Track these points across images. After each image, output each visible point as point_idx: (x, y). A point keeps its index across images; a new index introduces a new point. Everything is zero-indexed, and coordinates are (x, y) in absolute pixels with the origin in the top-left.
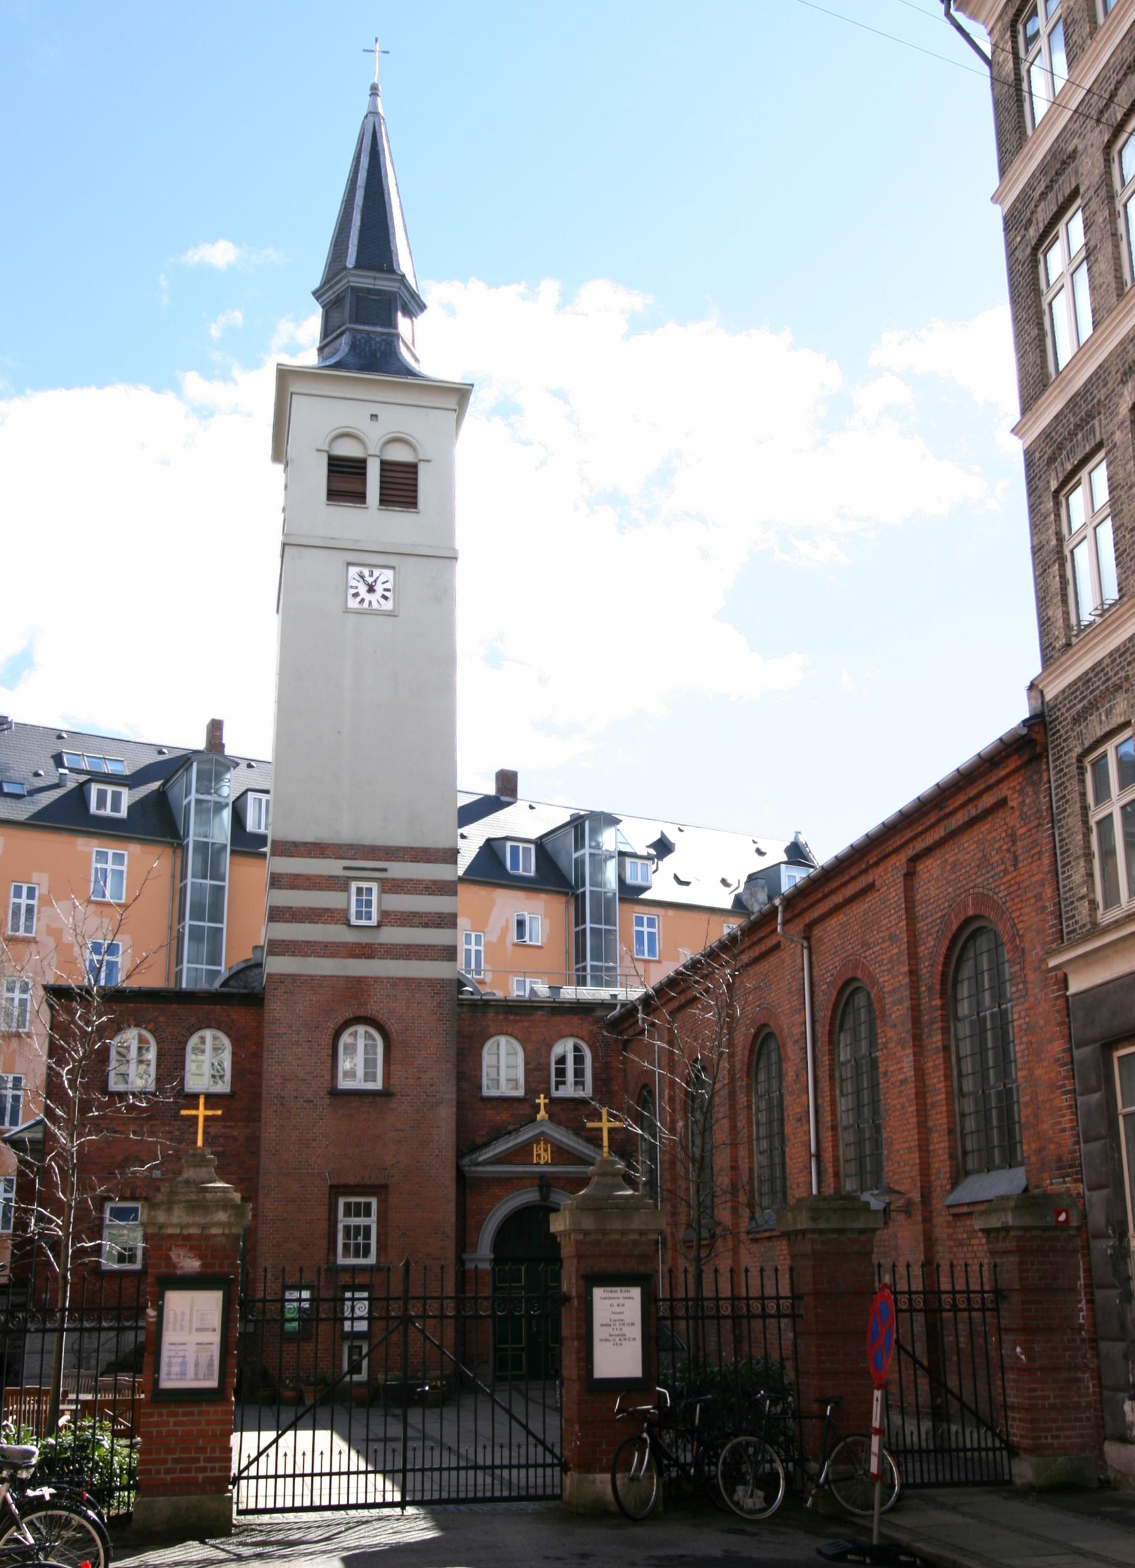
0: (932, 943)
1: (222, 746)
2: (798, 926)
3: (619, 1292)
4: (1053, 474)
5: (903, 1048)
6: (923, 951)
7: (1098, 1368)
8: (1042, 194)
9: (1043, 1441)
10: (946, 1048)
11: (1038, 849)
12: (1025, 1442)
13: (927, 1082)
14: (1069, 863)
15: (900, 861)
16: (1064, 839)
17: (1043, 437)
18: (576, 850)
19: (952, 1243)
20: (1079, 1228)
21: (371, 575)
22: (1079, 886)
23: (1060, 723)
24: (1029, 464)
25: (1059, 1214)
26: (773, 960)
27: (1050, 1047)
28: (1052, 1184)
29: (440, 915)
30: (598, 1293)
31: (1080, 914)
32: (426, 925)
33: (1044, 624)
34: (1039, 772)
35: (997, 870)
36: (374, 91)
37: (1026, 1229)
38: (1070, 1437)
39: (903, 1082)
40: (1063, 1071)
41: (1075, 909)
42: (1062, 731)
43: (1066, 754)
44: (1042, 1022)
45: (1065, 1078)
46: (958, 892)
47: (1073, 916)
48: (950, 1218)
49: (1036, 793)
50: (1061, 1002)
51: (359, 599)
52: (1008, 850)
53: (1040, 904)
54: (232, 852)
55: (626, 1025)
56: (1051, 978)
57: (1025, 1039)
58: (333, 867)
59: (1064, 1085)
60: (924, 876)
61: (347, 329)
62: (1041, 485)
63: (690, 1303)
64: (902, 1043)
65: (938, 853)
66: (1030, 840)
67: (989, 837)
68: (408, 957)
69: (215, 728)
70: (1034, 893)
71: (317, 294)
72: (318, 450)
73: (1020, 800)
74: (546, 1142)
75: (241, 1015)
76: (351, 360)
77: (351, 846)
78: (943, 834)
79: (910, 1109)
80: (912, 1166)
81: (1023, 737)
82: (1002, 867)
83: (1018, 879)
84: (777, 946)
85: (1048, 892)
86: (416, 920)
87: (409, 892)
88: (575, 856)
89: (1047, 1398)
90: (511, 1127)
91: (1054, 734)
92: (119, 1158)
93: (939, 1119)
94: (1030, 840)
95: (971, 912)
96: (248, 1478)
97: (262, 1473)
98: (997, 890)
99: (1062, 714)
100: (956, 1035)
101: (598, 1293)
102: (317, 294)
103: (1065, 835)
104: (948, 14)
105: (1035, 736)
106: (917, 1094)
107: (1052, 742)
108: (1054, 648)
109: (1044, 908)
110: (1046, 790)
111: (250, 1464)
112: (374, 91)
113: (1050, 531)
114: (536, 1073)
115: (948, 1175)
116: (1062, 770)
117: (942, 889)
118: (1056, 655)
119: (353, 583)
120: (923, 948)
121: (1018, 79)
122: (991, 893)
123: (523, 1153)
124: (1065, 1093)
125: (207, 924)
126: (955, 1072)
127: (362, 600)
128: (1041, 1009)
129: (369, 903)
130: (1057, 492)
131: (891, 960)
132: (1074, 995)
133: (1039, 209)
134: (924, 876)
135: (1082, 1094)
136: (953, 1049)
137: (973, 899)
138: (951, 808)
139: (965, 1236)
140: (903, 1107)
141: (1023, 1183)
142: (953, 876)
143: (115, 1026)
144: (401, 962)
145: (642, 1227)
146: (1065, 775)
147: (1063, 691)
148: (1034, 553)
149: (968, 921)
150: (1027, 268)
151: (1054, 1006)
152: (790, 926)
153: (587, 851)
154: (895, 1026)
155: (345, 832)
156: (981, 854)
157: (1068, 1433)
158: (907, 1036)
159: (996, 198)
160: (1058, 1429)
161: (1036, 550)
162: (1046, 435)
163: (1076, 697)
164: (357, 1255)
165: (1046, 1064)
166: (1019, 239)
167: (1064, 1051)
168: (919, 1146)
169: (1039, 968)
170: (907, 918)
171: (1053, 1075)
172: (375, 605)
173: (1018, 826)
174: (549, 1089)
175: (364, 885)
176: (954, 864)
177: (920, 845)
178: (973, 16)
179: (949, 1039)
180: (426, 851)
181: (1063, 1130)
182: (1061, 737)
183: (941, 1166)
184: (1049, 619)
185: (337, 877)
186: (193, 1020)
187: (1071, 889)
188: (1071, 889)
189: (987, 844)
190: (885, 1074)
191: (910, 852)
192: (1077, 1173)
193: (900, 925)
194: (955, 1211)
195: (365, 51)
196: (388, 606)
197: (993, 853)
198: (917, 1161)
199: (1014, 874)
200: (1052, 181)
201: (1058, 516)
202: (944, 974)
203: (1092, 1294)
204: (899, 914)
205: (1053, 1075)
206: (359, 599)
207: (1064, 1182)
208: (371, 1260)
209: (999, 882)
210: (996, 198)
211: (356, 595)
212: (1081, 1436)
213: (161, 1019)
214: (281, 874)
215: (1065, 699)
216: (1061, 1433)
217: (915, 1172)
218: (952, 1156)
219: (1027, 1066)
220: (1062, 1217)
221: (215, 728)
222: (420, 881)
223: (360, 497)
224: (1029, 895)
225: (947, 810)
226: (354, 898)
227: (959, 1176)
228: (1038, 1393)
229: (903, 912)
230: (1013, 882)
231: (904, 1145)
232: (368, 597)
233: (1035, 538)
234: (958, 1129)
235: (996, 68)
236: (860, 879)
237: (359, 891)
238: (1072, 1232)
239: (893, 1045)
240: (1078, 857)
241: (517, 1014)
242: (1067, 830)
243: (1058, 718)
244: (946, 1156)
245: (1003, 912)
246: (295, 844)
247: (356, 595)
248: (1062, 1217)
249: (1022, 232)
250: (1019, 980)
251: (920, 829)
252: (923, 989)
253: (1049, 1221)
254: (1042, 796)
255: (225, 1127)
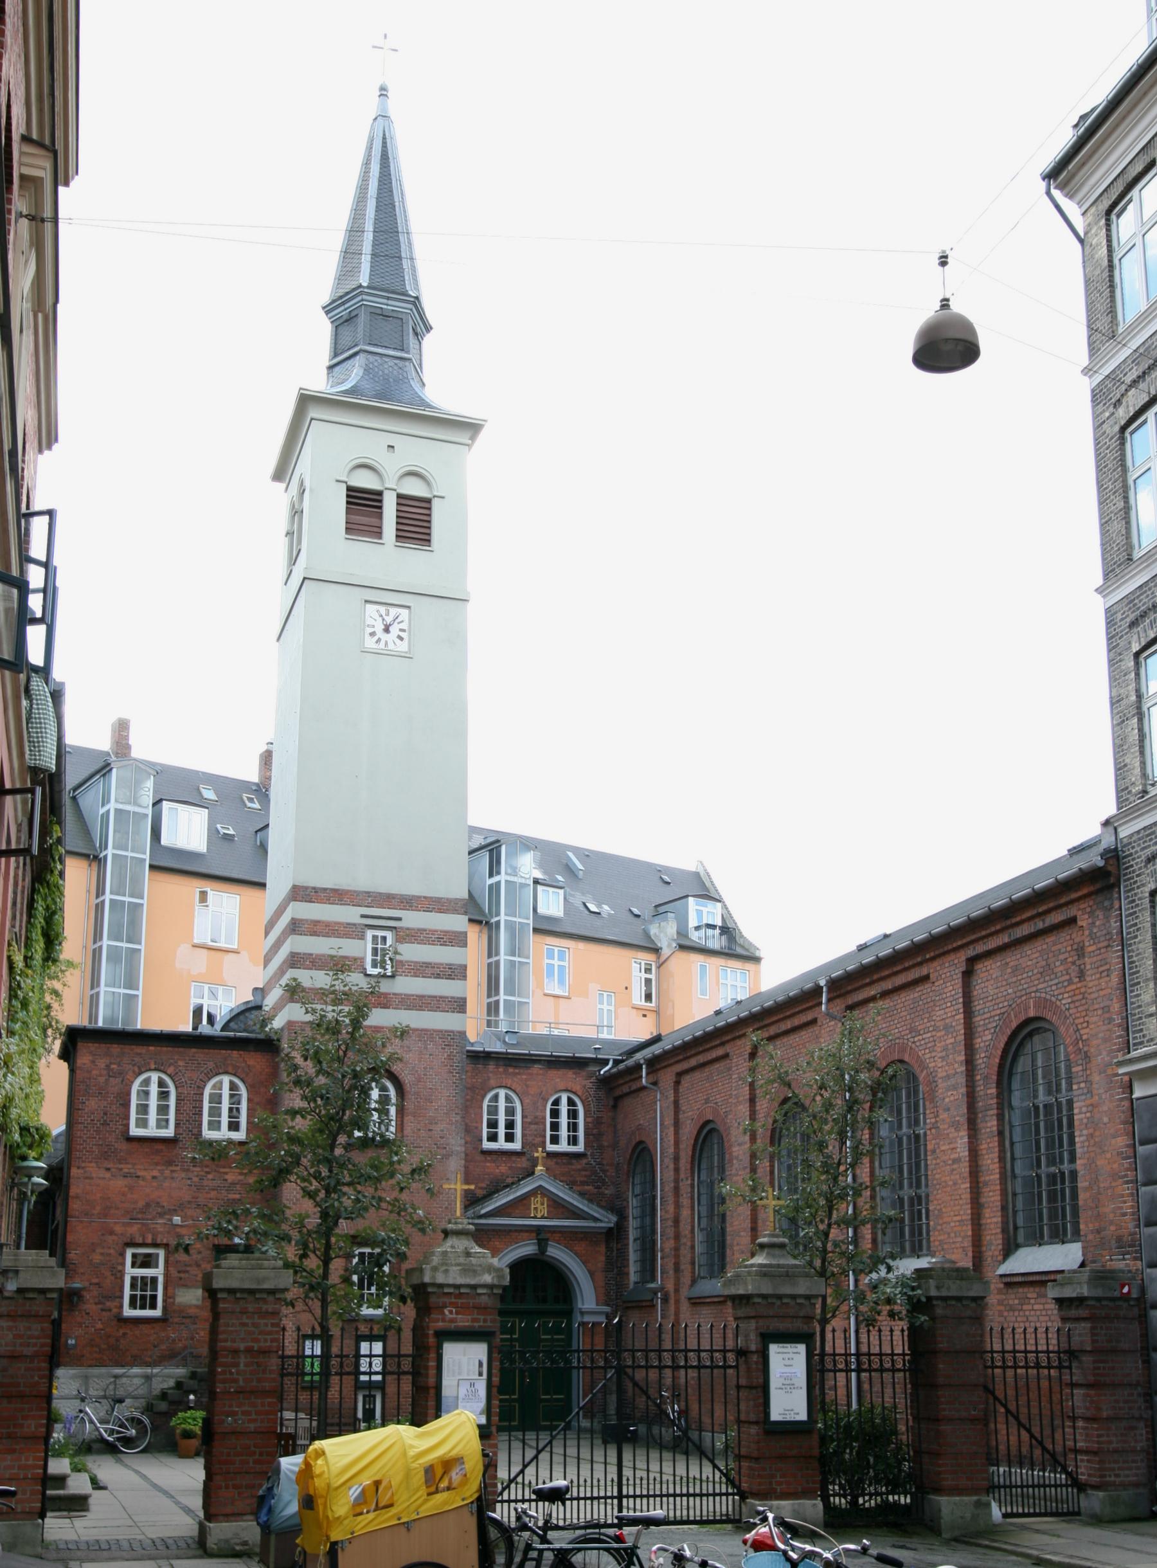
0: (990, 1037)
1: (129, 747)
2: (839, 1005)
3: (790, 1348)
4: (1135, 637)
5: (957, 1130)
6: (979, 1043)
7: (1153, 1418)
8: (1134, 382)
9: (1108, 1479)
10: (1001, 1133)
11: (1107, 967)
12: (1095, 1480)
13: (980, 1163)
14: (1139, 983)
15: (961, 958)
16: (1133, 962)
17: (1126, 601)
18: (491, 875)
19: (1002, 1308)
20: (1137, 1299)
21: (388, 614)
22: (1148, 1005)
23: (1134, 859)
24: (1110, 623)
25: (1123, 1286)
26: (804, 1034)
27: (1113, 1141)
28: (1111, 1260)
29: (450, 966)
30: (773, 1348)
31: (1148, 1029)
32: (438, 976)
33: (1121, 769)
34: (1111, 899)
35: (1061, 979)
36: (383, 92)
37: (1099, 1299)
38: (1128, 1476)
39: (957, 1161)
40: (1126, 1163)
41: (1143, 1024)
42: (1135, 867)
43: (1138, 887)
44: (1106, 1120)
45: (1127, 1169)
46: (1018, 994)
47: (1141, 1030)
48: (1002, 1286)
49: (1107, 918)
50: (1126, 1103)
51: (376, 638)
52: (1073, 963)
53: (1107, 1015)
54: (152, 867)
55: (621, 1082)
56: (1117, 1081)
57: (1085, 1132)
58: (350, 914)
59: (1126, 1176)
60: (982, 975)
61: (361, 351)
62: (1122, 643)
63: (682, 1363)
64: (956, 1125)
65: (998, 957)
66: (1099, 957)
67: (1053, 949)
68: (420, 1008)
69: (121, 729)
70: (1102, 1005)
71: (328, 309)
72: (338, 481)
73: (1090, 921)
74: (543, 1195)
75: (255, 1061)
76: (366, 385)
77: (368, 894)
78: (1006, 940)
79: (963, 1186)
80: (963, 1238)
81: (1100, 868)
82: (1067, 977)
83: (1083, 990)
84: (814, 1021)
85: (1116, 1006)
86: (429, 971)
87: (421, 942)
88: (490, 881)
89: (1110, 1442)
90: (509, 1180)
91: (1127, 868)
92: (141, 1204)
93: (992, 1197)
94: (1099, 957)
95: (1032, 1014)
96: (502, 1502)
97: (513, 1497)
98: (1060, 997)
99: (1136, 852)
100: (1010, 1122)
101: (773, 1348)
102: (328, 309)
103: (1135, 959)
104: (1048, 193)
105: (1110, 868)
106: (970, 1173)
107: (1125, 875)
108: (1130, 792)
109: (1111, 1020)
110: (1116, 916)
111: (504, 1489)
112: (383, 92)
113: (1130, 687)
114: (533, 1126)
115: (1000, 1247)
116: (1134, 901)
117: (1002, 989)
118: (1132, 799)
119: (369, 621)
120: (979, 1040)
121: (1111, 266)
122: (1053, 999)
123: (519, 1205)
124: (1127, 1182)
125: (125, 945)
126: (1009, 1155)
127: (379, 640)
128: (1105, 1108)
129: (375, 951)
130: (1137, 655)
131: (945, 1049)
132: (1138, 1099)
133: (1129, 393)
134: (982, 975)
135: (1145, 1185)
136: (1007, 1134)
137: (1035, 1003)
138: (1018, 919)
139: (1016, 1302)
140: (955, 1184)
141: (1080, 1258)
142: (1014, 979)
143: (136, 1069)
144: (414, 1013)
145: (808, 1293)
146: (1137, 905)
147: (1138, 832)
148: (1112, 704)
149: (1028, 1021)
150: (1114, 443)
151: (1118, 1106)
152: (831, 1005)
153: (502, 878)
154: (948, 1110)
155: (362, 881)
156: (1044, 963)
157: (1127, 1472)
158: (963, 1120)
159: (1087, 371)
160: (1120, 1469)
161: (1115, 702)
162: (1129, 600)
163: (1151, 840)
164: (143, 1307)
165: (1108, 1156)
166: (1107, 414)
167: (1127, 1146)
168: (972, 1219)
169: (1105, 1071)
170: (964, 1012)
171: (1115, 1166)
172: (391, 646)
173: (1087, 944)
174: (544, 1142)
175: (380, 933)
176: (1015, 969)
177: (980, 948)
178: (1070, 196)
179: (1003, 1125)
180: (438, 900)
181: (1124, 1215)
182: (1134, 872)
183: (993, 1239)
184: (1125, 765)
185: (354, 925)
186: (211, 1065)
187: (1140, 1006)
188: (1140, 1006)
189: (1051, 955)
190: (934, 1151)
191: (970, 952)
192: (1136, 1252)
193: (957, 1017)
194: (1008, 1280)
195: (374, 47)
196: (403, 647)
197: (1058, 964)
198: (970, 1233)
199: (1079, 985)
200: (1144, 373)
201: (1138, 675)
202: (1001, 1066)
203: (1148, 1355)
204: (956, 1007)
205: (1115, 1166)
206: (376, 638)
207: (1124, 1259)
208: (157, 1313)
209: (1063, 990)
210: (1087, 371)
211: (373, 634)
212: (1136, 1475)
213: (181, 1063)
214: (302, 920)
215: (1140, 839)
216: (1121, 1473)
217: (968, 1243)
218: (1005, 1230)
219: (1087, 1156)
220: (1126, 1290)
221: (121, 729)
222: (434, 932)
223: (378, 533)
224: (1096, 1006)
225: (1014, 920)
226: (370, 946)
227: (1009, 1249)
228: (1104, 1439)
229: (961, 1006)
230: (1077, 992)
231: (956, 1218)
232: (384, 637)
233: (1114, 690)
234: (1011, 1206)
235: (1087, 248)
236: (913, 970)
237: (375, 938)
238: (1132, 1303)
239: (946, 1126)
240: (1148, 980)
241: (516, 1067)
242: (1137, 955)
243: (1131, 855)
244: (999, 1230)
245: (1066, 1018)
246: (316, 890)
247: (373, 634)
248: (1126, 1290)
249: (1111, 409)
250: (1081, 1079)
251: (984, 933)
252: (978, 1077)
253: (1117, 1294)
254: (1112, 921)
255: (241, 1174)
